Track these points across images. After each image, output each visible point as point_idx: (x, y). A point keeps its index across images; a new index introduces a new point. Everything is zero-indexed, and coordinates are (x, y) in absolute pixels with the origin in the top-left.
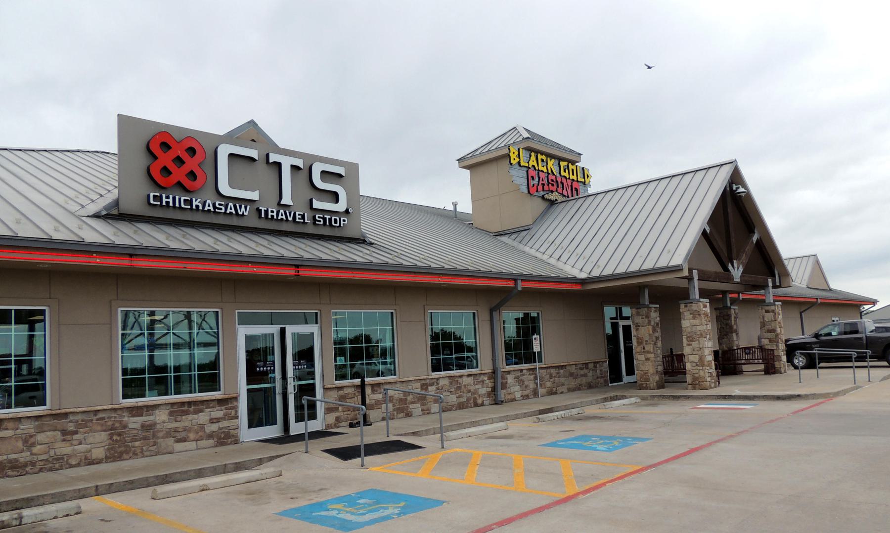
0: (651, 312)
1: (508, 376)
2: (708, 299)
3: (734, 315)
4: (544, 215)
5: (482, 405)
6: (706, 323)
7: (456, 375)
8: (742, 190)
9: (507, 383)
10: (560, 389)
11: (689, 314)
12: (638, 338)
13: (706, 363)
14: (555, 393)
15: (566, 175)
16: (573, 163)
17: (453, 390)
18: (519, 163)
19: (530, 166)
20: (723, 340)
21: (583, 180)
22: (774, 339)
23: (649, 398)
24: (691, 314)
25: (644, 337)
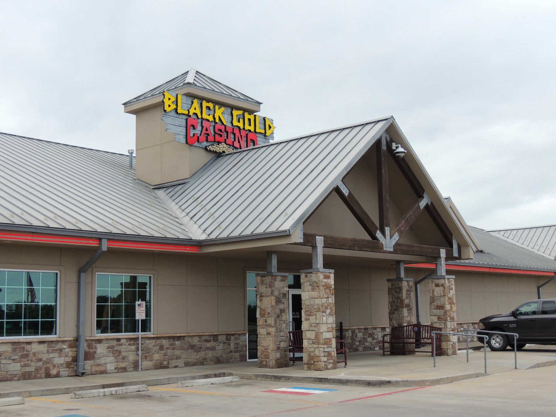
0: (276, 280)
1: (98, 345)
2: (81, 273)
3: (407, 287)
4: (205, 167)
5: (57, 376)
6: (326, 296)
7: (21, 341)
8: (401, 149)
9: (95, 352)
10: (173, 363)
11: (308, 285)
12: (261, 310)
13: (322, 341)
14: (167, 367)
15: (241, 125)
16: (251, 112)
17: (17, 357)
18: (176, 110)
19: (191, 114)
20: (394, 315)
21: (263, 131)
22: (443, 317)
23: (253, 377)
24: (310, 285)
25: (266, 308)
